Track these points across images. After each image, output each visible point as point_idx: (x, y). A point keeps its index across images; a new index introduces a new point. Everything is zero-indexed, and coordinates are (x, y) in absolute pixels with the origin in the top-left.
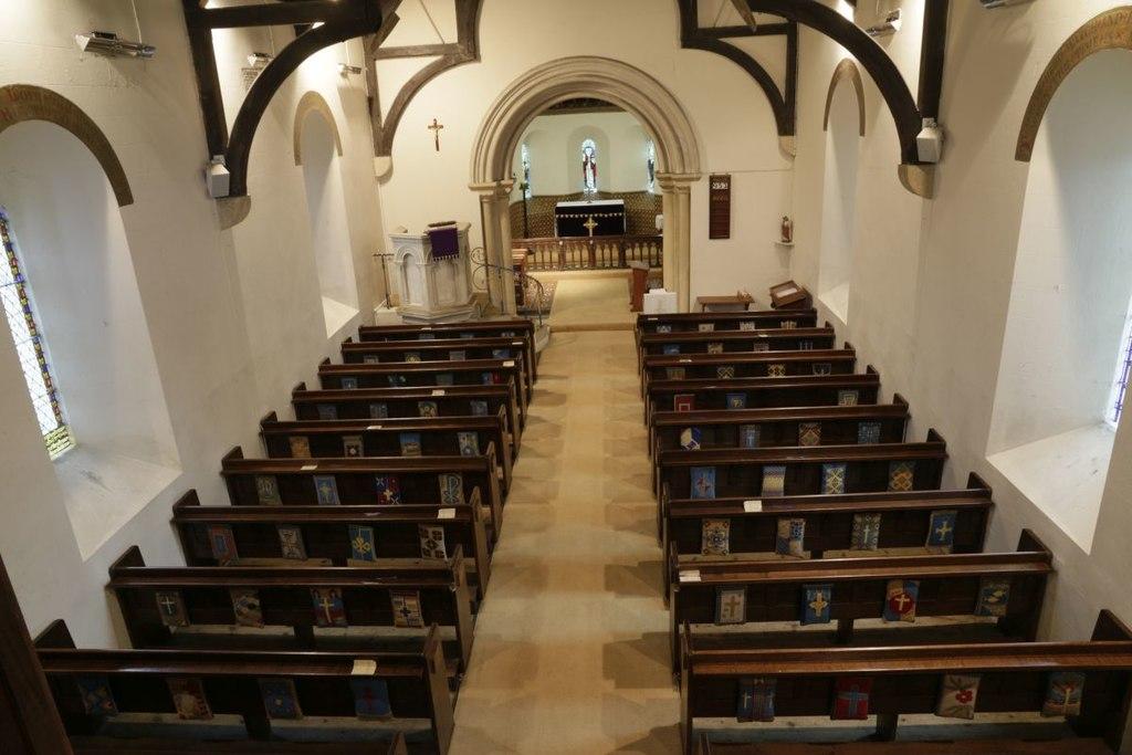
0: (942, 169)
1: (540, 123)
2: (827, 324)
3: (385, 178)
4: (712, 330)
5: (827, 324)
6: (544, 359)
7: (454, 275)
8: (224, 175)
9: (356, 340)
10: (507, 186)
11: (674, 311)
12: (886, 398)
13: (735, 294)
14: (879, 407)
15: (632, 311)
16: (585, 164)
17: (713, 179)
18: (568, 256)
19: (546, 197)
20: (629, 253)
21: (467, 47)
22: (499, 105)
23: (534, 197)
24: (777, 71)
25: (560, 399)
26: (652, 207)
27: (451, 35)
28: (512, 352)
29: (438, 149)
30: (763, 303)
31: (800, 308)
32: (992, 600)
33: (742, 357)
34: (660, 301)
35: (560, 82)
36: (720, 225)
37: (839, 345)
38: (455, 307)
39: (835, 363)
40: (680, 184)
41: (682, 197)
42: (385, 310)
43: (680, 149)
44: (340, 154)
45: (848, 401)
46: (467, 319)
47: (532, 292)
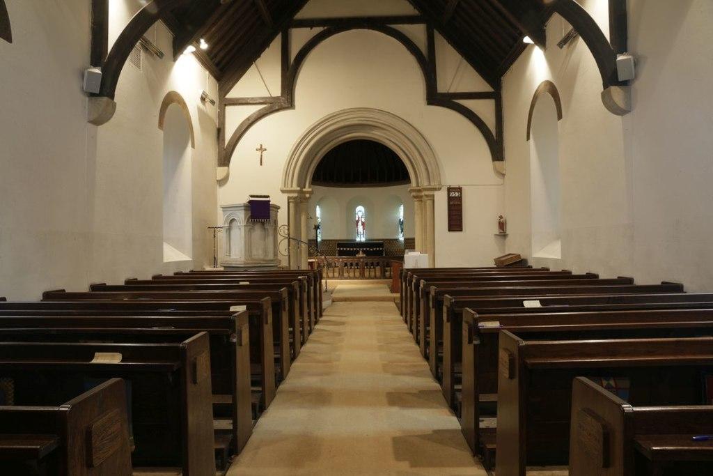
0: (637, 85)
3: (223, 182)
7: (265, 238)
10: (308, 192)
11: (426, 266)
16: (358, 222)
17: (450, 190)
19: (332, 240)
21: (287, 100)
22: (305, 136)
24: (490, 121)
27: (276, 91)
29: (261, 164)
36: (455, 222)
38: (264, 260)
40: (427, 193)
41: (429, 203)
43: (427, 169)
44: (193, 146)
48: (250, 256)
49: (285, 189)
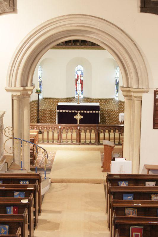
4: (154, 186)
15: (103, 171)
16: (77, 80)
18: (64, 136)
20: (101, 135)
23: (44, 99)
26: (117, 109)
28: (27, 194)
40: (135, 95)
41: (137, 103)
43: (137, 73)
47: (40, 156)
49: (9, 88)
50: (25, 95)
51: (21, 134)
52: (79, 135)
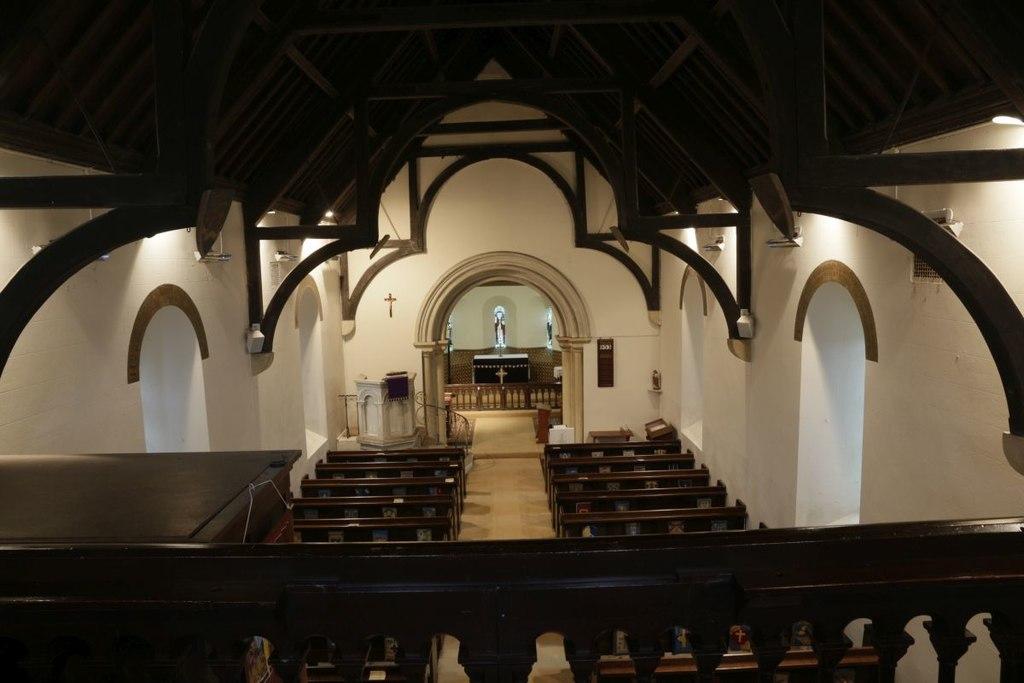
0: (757, 342)
1: (477, 296)
2: (688, 451)
3: (349, 337)
4: (602, 456)
5: (688, 451)
6: (469, 476)
7: (404, 412)
8: (259, 338)
9: (325, 462)
10: (444, 345)
11: (572, 442)
12: (731, 503)
13: (618, 429)
14: (728, 509)
15: (538, 443)
16: (497, 325)
17: (600, 342)
18: (485, 398)
20: (533, 396)
23: (455, 351)
25: (485, 510)
26: (550, 360)
28: (452, 472)
30: (640, 436)
31: (667, 439)
32: (801, 633)
33: (626, 475)
34: (560, 434)
35: (485, 269)
36: (606, 377)
37: (698, 467)
38: (404, 437)
39: (694, 479)
40: (575, 346)
41: (577, 355)
42: (345, 439)
43: (575, 319)
45: (705, 505)
46: (411, 447)
47: (458, 426)
48: (389, 434)
50: (437, 350)
51: (435, 399)
52: (504, 397)
